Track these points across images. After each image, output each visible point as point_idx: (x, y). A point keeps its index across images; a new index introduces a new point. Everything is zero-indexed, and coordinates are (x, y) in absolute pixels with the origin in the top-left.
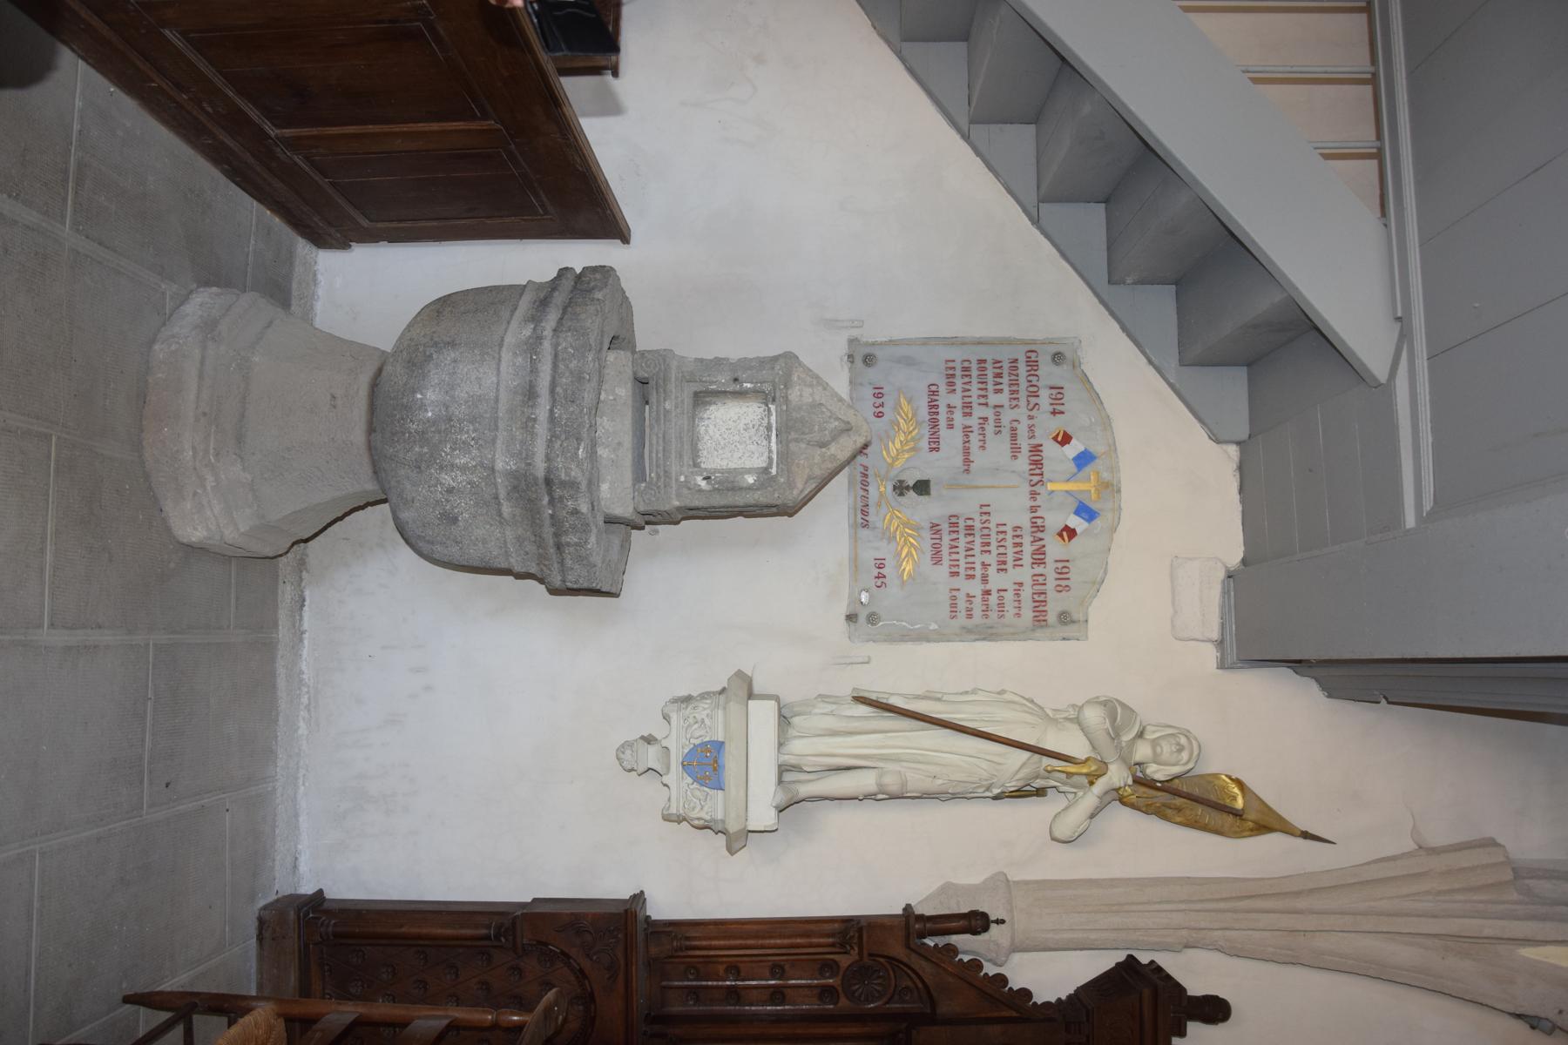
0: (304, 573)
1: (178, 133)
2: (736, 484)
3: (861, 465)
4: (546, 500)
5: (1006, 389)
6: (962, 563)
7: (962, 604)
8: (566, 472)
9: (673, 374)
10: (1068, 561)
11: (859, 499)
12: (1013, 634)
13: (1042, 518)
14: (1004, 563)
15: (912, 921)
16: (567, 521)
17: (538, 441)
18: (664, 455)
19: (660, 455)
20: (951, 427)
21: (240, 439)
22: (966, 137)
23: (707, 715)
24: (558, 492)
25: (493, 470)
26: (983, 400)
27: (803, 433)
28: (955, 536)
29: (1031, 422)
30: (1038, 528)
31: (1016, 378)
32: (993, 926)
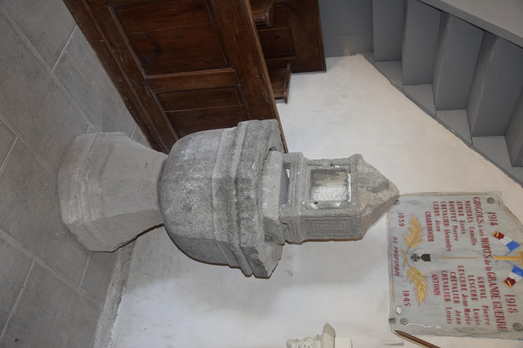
1: (109, 74)
2: (331, 206)
3: (394, 247)
4: (234, 193)
5: (465, 214)
6: (451, 294)
7: (454, 316)
8: (245, 175)
9: (302, 162)
10: (513, 296)
11: (394, 263)
12: (487, 334)
13: (494, 273)
16: (244, 204)
17: (234, 163)
18: (295, 193)
19: (294, 193)
20: (439, 230)
21: (101, 172)
22: (435, 117)
23: (312, 344)
24: (240, 186)
25: (211, 179)
26: (454, 219)
27: (365, 184)
28: (446, 281)
29: (480, 228)
31: (470, 209)
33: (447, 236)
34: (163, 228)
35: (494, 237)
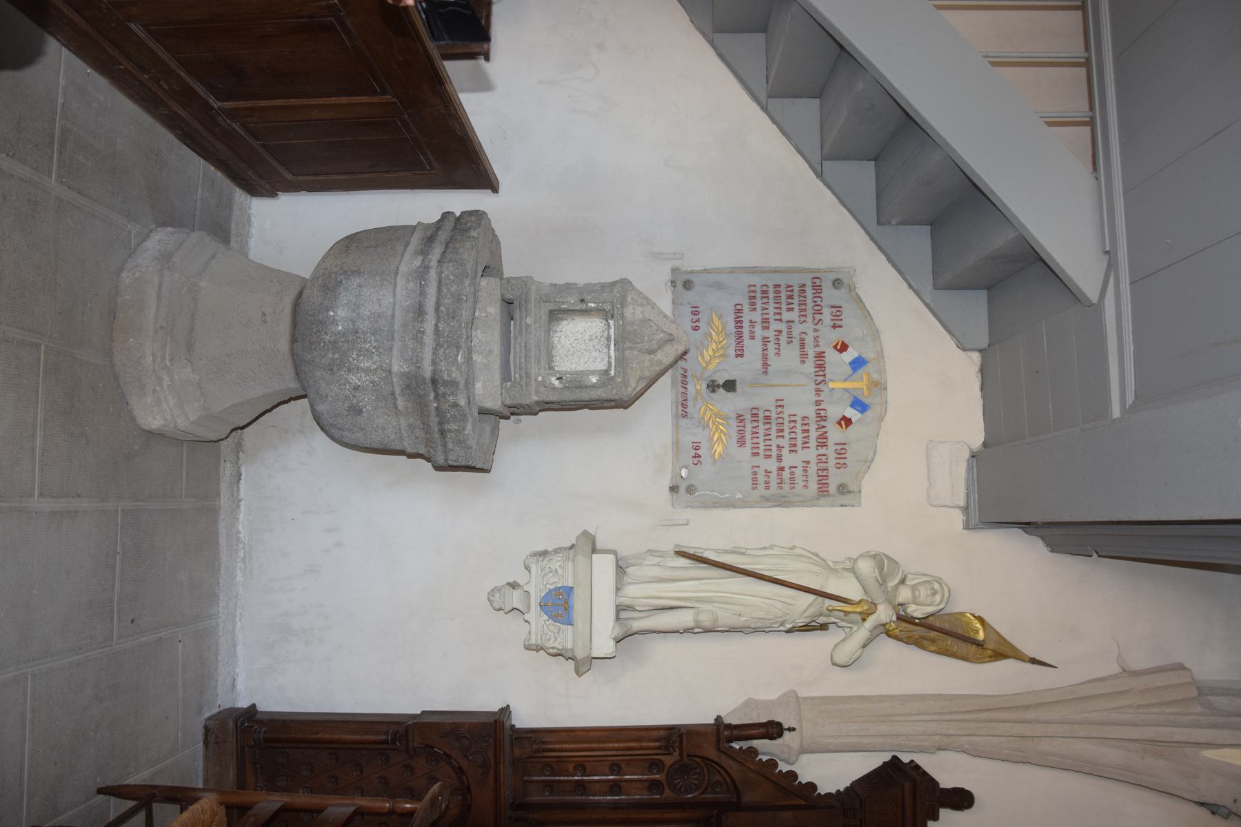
0: (241, 454)
1: (141, 105)
2: (582, 383)
3: (682, 368)
4: (432, 395)
7: (761, 478)
8: (448, 374)
10: (845, 444)
14: (795, 445)
15: (722, 729)
17: (426, 349)
18: (525, 360)
19: (523, 360)
20: (752, 338)
21: (190, 347)
22: (765, 109)
24: (442, 390)
25: (390, 372)
26: (778, 317)
27: (636, 343)
29: (816, 334)
30: (821, 418)
31: (804, 299)
32: (786, 733)
33: (765, 348)
34: (306, 400)
35: (833, 349)
